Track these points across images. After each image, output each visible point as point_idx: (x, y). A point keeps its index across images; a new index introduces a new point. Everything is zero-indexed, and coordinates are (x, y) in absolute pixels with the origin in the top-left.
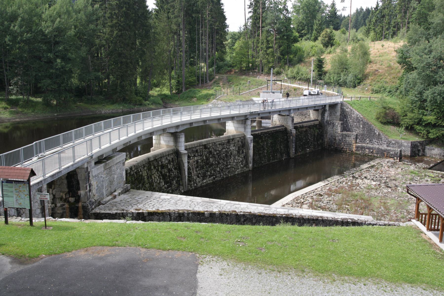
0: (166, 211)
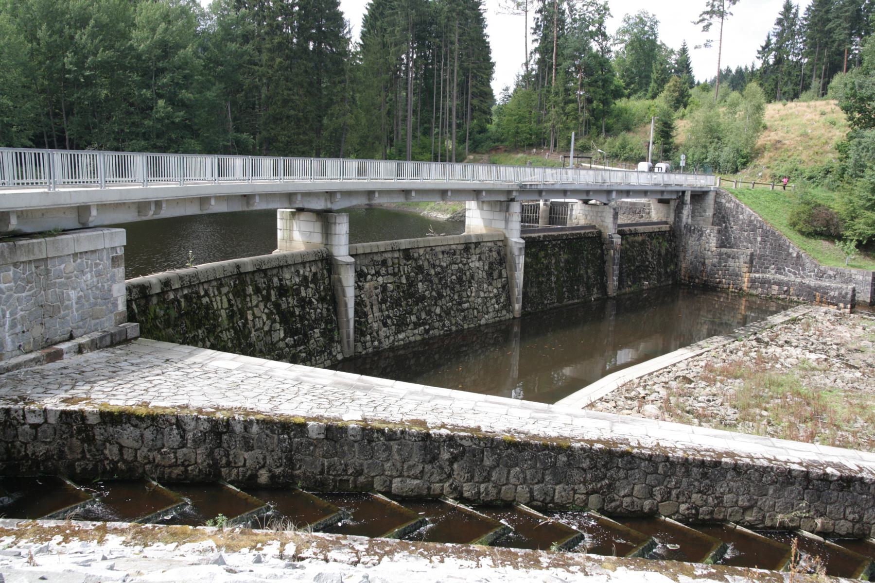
0: (168, 411)
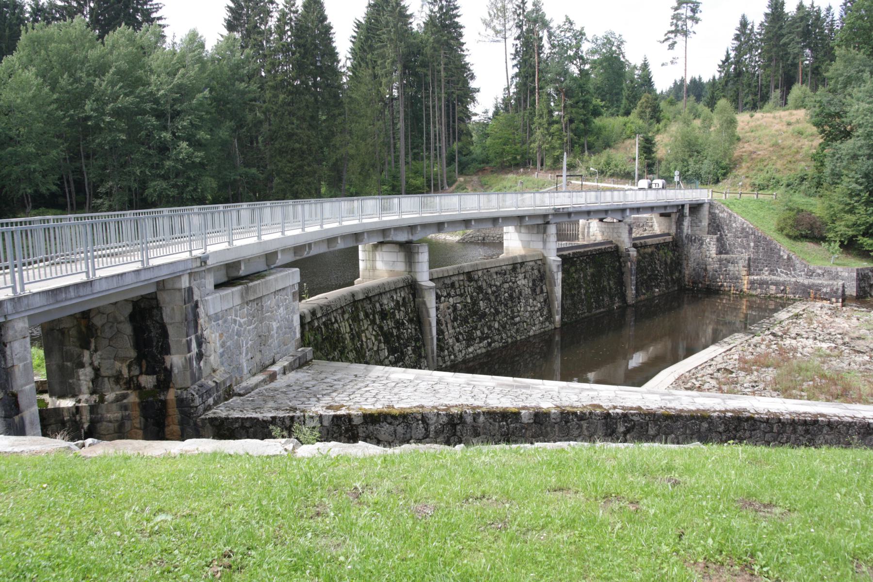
0: (415, 410)
